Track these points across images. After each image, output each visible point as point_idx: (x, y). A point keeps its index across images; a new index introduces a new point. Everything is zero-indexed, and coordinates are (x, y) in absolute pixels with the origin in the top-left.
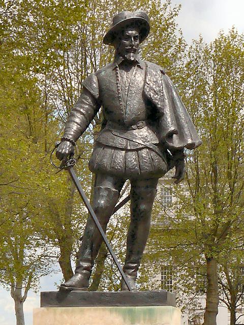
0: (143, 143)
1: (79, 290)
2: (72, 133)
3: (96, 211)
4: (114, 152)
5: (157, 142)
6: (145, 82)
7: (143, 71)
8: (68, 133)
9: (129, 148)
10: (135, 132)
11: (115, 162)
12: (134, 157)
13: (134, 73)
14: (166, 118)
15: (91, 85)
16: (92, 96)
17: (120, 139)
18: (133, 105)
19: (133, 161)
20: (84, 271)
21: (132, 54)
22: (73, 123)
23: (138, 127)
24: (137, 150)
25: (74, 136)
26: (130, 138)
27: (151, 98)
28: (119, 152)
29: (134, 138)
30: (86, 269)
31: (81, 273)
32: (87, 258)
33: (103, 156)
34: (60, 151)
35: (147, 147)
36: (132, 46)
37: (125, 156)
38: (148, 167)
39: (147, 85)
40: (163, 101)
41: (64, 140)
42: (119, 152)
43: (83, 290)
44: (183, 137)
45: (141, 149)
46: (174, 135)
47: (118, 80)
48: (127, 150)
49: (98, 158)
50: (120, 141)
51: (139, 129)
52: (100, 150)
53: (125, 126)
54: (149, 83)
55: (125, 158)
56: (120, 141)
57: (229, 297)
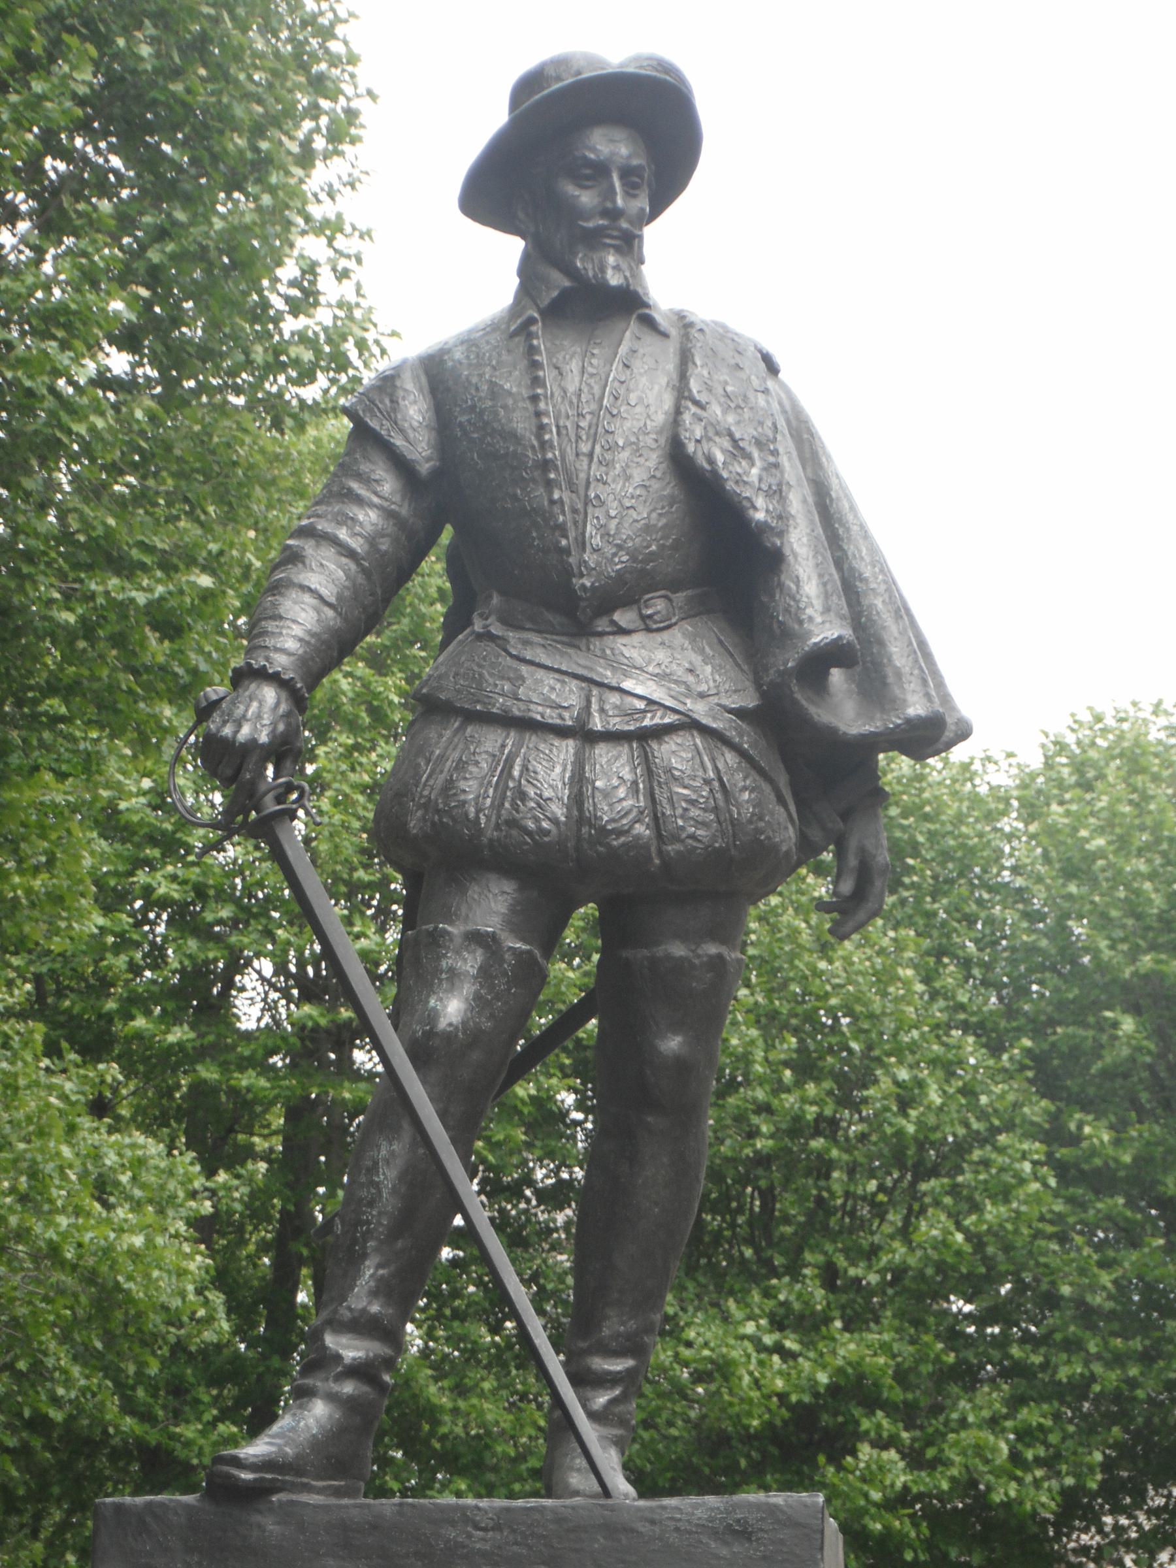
0: (669, 702)
1: (319, 1491)
2: (291, 645)
3: (420, 1054)
4: (518, 745)
5: (750, 701)
6: (682, 392)
7: (671, 349)
8: (269, 642)
9: (599, 727)
10: (631, 648)
11: (523, 796)
12: (626, 773)
13: (623, 350)
14: (797, 581)
15: (392, 414)
16: (401, 465)
17: (550, 680)
18: (619, 508)
19: (621, 792)
20: (348, 1388)
21: (611, 259)
22: (294, 594)
23: (644, 618)
24: (645, 736)
25: (303, 662)
26: (609, 676)
27: (715, 473)
28: (542, 746)
29: (626, 675)
30: (356, 1371)
31: (332, 1398)
32: (364, 1311)
33: (461, 766)
34: (227, 731)
35: (691, 725)
36: (614, 214)
37: (579, 765)
38: (704, 824)
39: (694, 409)
40: (778, 493)
41: (242, 677)
42: (542, 746)
43: (338, 1492)
44: (885, 684)
45: (660, 732)
46: (836, 676)
47: (537, 381)
48: (586, 736)
49: (431, 784)
50: (549, 691)
51: (649, 630)
52: (442, 737)
53: (578, 611)
54: (702, 398)
55: (579, 780)
56: (549, 691)
57: (783, 780)
